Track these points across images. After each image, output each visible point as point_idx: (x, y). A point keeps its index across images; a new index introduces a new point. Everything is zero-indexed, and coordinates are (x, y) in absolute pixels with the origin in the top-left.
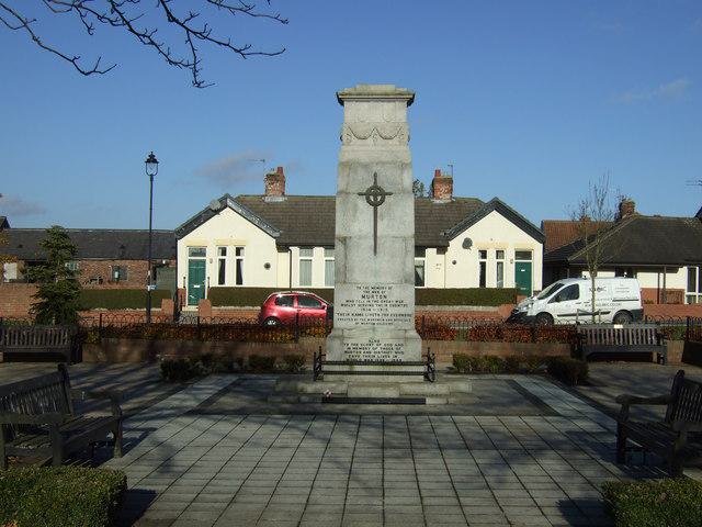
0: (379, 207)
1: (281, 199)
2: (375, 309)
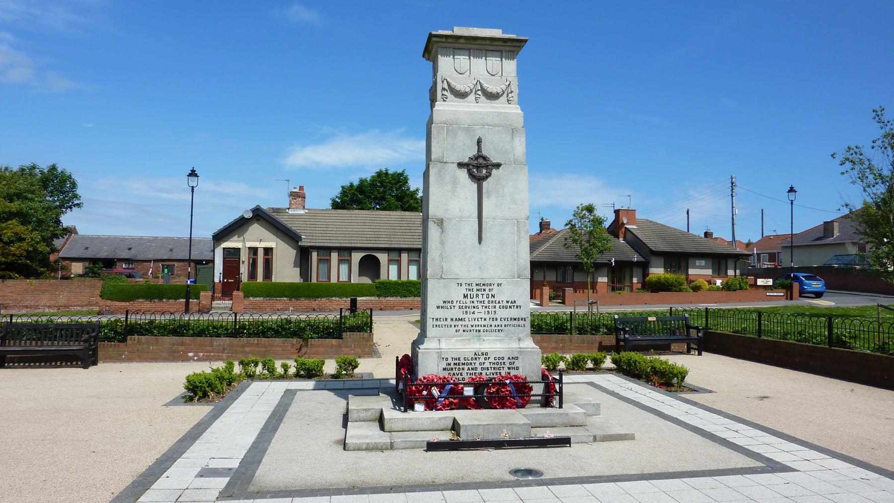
0: (485, 184)
1: (302, 212)
2: (480, 313)
